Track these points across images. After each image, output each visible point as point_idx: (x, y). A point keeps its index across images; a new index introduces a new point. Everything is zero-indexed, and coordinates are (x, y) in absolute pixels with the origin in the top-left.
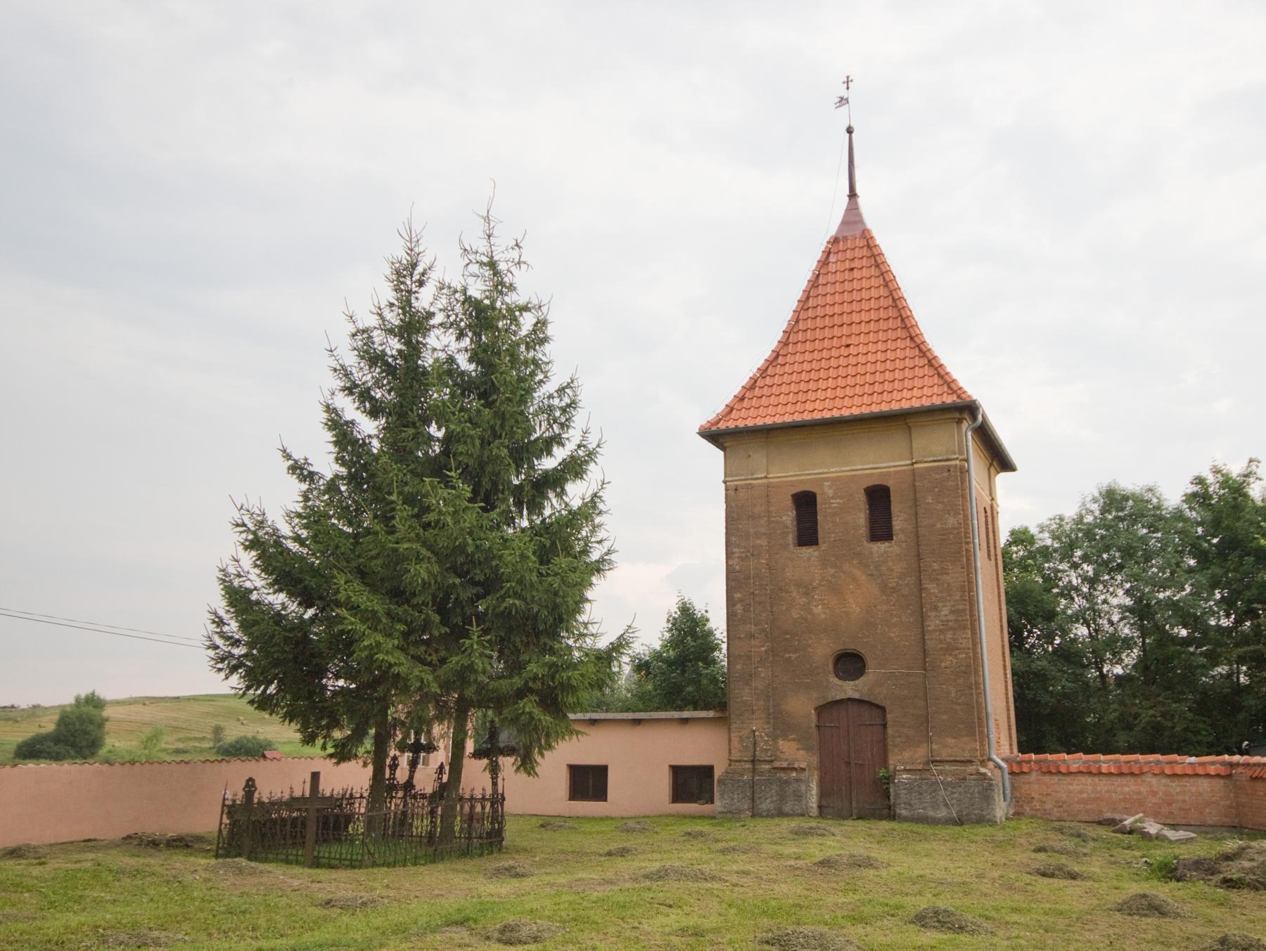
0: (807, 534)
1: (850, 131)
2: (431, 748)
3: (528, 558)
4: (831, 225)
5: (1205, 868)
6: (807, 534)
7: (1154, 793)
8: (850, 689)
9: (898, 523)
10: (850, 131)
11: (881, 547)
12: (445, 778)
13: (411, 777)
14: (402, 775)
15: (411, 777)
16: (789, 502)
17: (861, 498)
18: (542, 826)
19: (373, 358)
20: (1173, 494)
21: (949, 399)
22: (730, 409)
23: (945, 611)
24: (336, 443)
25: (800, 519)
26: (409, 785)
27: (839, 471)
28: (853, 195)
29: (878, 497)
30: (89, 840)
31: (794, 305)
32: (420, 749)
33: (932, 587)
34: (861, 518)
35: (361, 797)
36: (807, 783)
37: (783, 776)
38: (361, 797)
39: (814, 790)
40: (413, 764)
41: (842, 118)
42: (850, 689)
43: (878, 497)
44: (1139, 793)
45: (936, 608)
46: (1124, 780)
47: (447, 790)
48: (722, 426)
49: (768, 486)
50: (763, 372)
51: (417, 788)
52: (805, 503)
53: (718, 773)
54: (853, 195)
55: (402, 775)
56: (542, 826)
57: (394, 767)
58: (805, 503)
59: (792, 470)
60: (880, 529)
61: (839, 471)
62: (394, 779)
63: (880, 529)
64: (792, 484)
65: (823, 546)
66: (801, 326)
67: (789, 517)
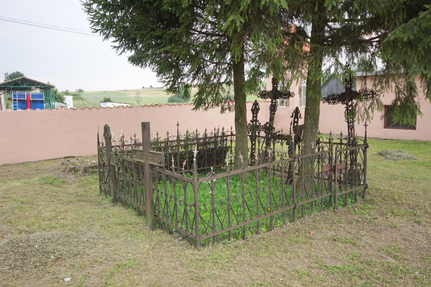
1: (178, 125)
2: (288, 95)
5: (365, 152)
12: (301, 122)
13: (272, 119)
14: (263, 118)
15: (272, 119)
18: (381, 154)
19: (142, 65)
24: (167, 142)
26: (269, 128)
30: (5, 165)
32: (278, 94)
35: (232, 135)
38: (232, 135)
40: (273, 108)
47: (305, 129)
51: (276, 130)
55: (263, 118)
56: (381, 154)
57: (256, 110)
62: (256, 121)
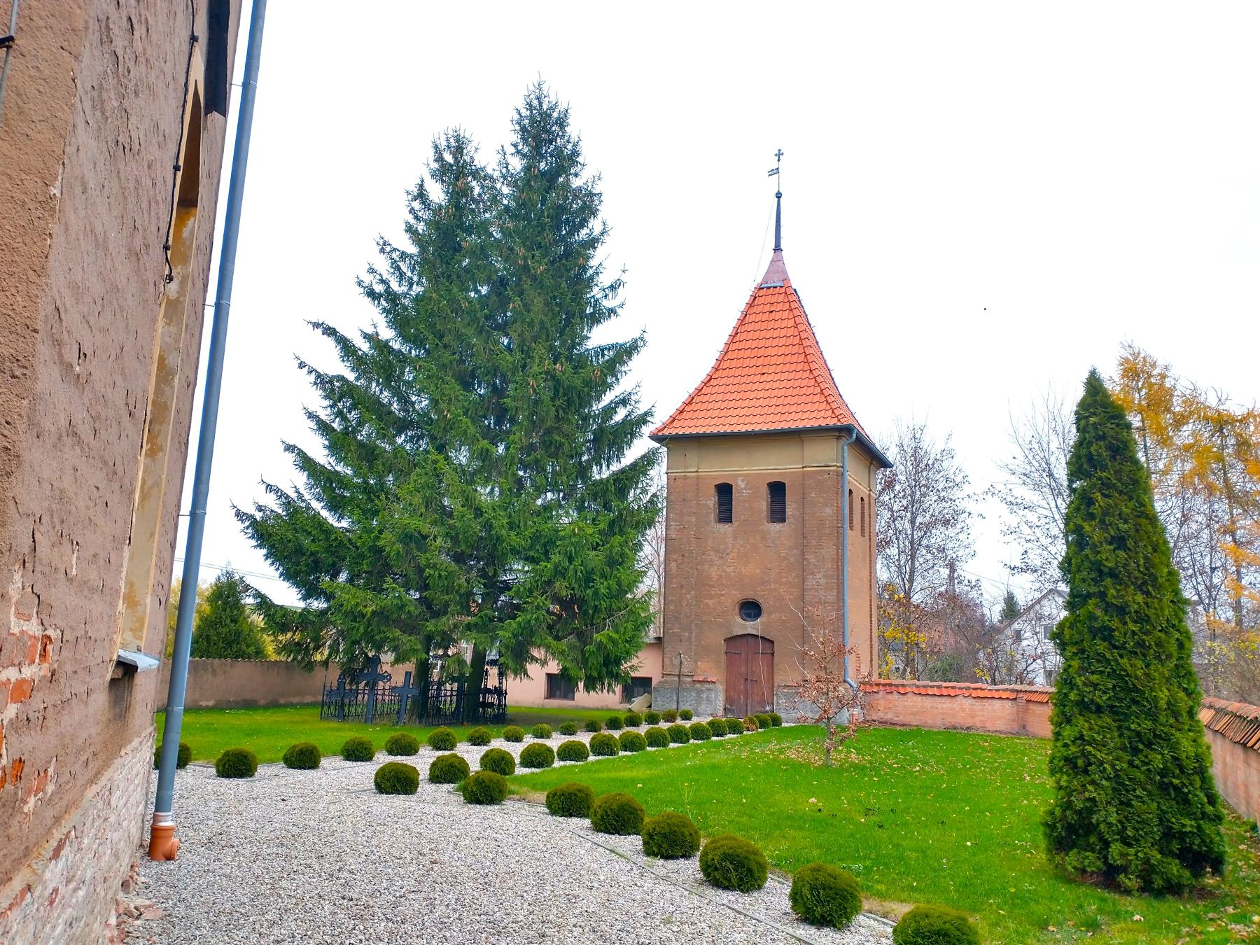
0: (725, 515)
1: (779, 196)
3: (556, 566)
4: (754, 273)
6: (725, 515)
7: (963, 710)
8: (752, 627)
9: (790, 510)
10: (779, 196)
11: (777, 527)
16: (713, 491)
17: (765, 491)
20: (365, 321)
21: (832, 422)
22: (673, 419)
23: (819, 576)
25: (721, 502)
27: (750, 471)
28: (778, 248)
29: (777, 490)
31: (725, 339)
33: (811, 558)
34: (763, 504)
36: (716, 691)
37: (698, 685)
39: (721, 697)
41: (772, 185)
42: (752, 627)
43: (777, 490)
44: (952, 709)
45: (813, 574)
46: (943, 699)
48: (666, 432)
49: (697, 478)
50: (699, 391)
52: (725, 491)
53: (654, 683)
54: (778, 248)
58: (725, 491)
59: (717, 467)
60: (778, 514)
61: (750, 471)
63: (778, 514)
64: (715, 478)
65: (735, 524)
66: (729, 356)
67: (712, 501)
